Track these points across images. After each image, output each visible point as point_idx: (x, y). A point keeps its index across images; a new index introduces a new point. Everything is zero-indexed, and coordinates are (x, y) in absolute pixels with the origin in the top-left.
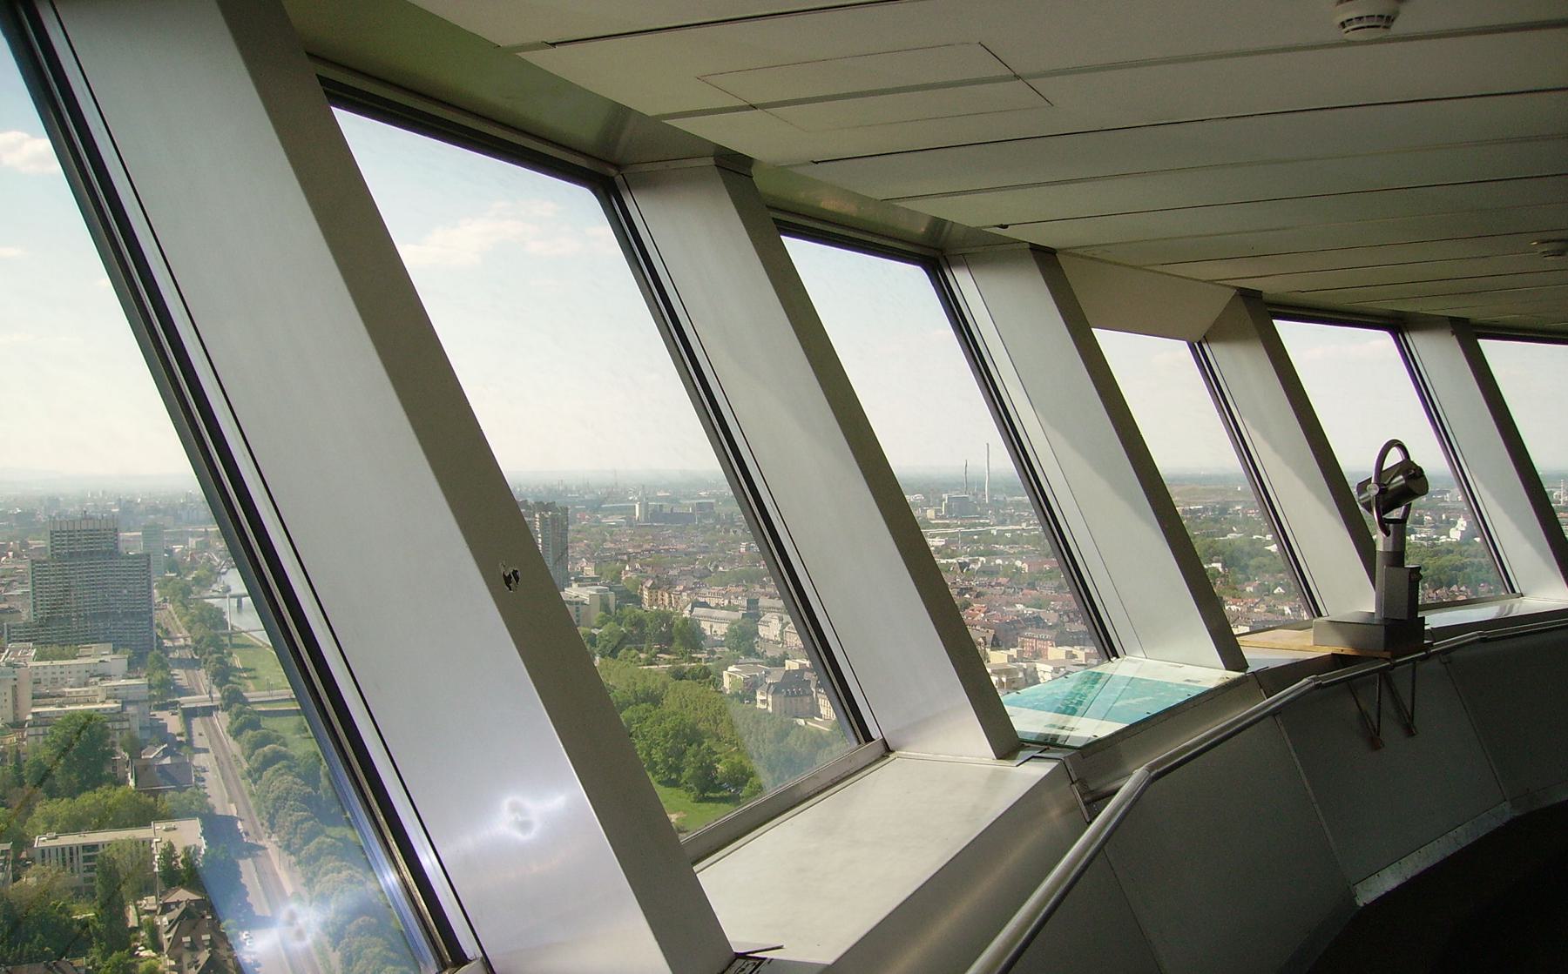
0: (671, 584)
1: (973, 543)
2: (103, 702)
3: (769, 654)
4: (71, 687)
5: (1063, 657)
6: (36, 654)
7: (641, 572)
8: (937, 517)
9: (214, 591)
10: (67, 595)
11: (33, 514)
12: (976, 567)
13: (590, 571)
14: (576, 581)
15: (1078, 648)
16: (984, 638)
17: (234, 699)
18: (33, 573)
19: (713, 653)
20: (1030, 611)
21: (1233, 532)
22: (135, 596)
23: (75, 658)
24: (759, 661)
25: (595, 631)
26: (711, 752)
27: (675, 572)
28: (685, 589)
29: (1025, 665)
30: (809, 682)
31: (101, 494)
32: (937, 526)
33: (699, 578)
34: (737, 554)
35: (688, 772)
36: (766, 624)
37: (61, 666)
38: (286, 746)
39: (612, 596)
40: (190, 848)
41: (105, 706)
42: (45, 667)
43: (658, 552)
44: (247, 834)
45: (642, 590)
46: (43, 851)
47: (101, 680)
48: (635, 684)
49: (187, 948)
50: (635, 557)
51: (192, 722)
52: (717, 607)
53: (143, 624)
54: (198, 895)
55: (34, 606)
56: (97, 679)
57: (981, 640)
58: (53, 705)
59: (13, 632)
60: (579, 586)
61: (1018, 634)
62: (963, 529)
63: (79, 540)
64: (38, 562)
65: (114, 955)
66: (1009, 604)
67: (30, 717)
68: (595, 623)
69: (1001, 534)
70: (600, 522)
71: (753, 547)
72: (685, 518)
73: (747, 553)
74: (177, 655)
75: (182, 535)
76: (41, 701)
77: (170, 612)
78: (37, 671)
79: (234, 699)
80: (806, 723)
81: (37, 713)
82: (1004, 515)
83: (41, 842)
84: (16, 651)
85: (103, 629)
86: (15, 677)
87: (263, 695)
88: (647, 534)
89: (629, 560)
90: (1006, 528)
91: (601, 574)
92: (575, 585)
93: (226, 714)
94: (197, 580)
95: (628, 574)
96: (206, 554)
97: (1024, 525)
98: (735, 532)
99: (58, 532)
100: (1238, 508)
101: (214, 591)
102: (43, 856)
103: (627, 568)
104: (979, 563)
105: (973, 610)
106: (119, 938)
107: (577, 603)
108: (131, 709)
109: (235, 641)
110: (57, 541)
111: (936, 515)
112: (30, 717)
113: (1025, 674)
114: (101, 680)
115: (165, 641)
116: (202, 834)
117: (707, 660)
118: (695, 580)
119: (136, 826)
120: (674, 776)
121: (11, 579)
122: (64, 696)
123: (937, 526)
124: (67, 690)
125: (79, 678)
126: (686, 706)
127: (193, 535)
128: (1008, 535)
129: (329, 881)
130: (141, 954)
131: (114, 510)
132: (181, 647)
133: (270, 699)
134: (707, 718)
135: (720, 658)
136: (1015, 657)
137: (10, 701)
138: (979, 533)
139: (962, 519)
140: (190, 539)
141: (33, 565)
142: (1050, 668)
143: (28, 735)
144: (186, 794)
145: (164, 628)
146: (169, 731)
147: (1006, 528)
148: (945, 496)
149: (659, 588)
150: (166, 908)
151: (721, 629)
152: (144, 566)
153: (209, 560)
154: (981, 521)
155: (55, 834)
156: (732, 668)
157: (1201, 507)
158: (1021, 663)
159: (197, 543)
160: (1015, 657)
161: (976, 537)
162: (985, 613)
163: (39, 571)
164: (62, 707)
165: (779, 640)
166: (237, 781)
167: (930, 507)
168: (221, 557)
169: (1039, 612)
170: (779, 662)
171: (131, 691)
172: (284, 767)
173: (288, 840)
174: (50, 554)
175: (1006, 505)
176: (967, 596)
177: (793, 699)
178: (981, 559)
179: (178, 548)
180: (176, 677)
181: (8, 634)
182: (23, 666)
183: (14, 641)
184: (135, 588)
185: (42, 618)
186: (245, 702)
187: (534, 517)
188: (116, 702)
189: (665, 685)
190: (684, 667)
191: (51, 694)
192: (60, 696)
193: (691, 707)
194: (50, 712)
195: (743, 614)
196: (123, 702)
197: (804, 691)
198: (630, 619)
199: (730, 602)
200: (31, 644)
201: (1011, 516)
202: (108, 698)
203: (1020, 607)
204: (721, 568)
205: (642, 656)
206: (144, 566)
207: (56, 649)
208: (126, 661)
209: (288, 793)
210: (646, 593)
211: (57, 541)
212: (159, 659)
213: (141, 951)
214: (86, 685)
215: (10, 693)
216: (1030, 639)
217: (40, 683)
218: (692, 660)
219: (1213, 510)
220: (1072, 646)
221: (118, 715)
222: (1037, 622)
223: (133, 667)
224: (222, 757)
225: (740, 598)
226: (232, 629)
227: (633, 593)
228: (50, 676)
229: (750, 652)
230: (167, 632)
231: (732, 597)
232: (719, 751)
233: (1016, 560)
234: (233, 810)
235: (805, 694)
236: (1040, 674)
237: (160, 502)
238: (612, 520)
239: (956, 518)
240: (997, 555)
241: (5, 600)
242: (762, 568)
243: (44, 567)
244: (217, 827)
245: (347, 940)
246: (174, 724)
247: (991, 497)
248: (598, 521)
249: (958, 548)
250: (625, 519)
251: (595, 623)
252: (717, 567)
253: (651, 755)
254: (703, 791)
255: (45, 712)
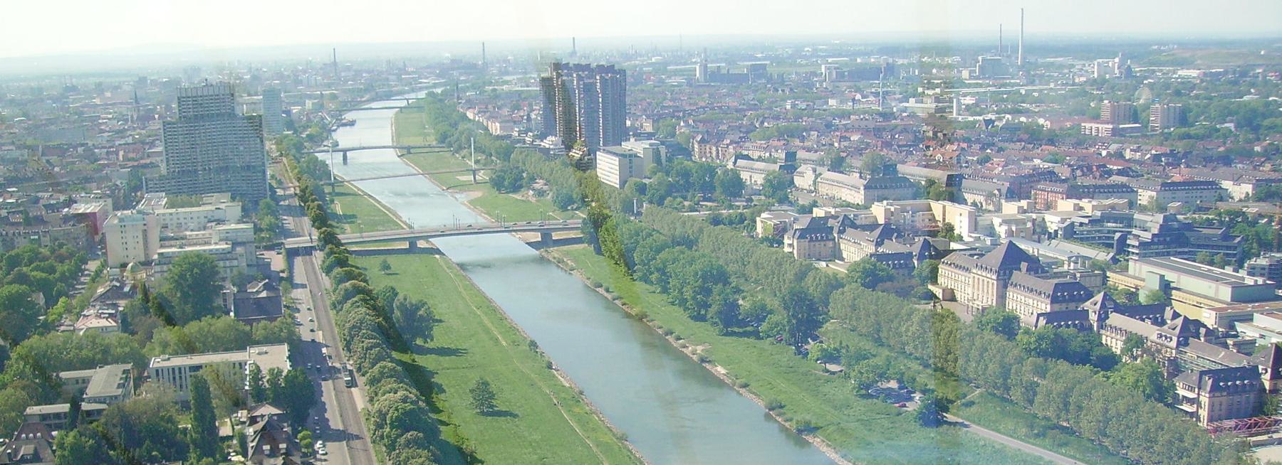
0: (720, 137)
1: (1001, 101)
2: (216, 244)
3: (801, 202)
4: (192, 230)
5: (1071, 209)
6: (166, 203)
7: (693, 127)
8: (970, 78)
9: (325, 146)
10: (194, 152)
11: (178, 82)
12: (999, 124)
13: (648, 127)
14: (634, 135)
15: (1086, 200)
16: (999, 190)
17: (329, 239)
18: (165, 133)
19: (752, 200)
20: (1047, 165)
21: (1251, 93)
22: (212, 150)
23: (200, 206)
24: (790, 208)
25: (646, 181)
26: (738, 291)
27: (725, 127)
28: (732, 142)
29: (1034, 216)
30: (832, 228)
31: (236, 64)
32: (969, 86)
33: (744, 133)
34: (784, 110)
35: (714, 309)
36: (802, 174)
37: (191, 213)
38: (366, 281)
39: (663, 150)
40: (274, 370)
41: (218, 247)
42: (171, 214)
43: (713, 109)
44: (330, 357)
45: (693, 144)
46: (157, 371)
47: (216, 224)
48: (675, 229)
49: (266, 455)
50: (690, 114)
51: (295, 260)
52: (760, 159)
53: (257, 176)
54: (279, 408)
55: (167, 162)
56: (213, 224)
57: (996, 192)
58: (175, 246)
59: (151, 184)
60: (636, 140)
61: (1031, 187)
62: (993, 89)
63: (201, 104)
64: (169, 124)
65: (204, 460)
66: (1026, 159)
67: (156, 257)
68: (648, 174)
69: (1028, 93)
70: (663, 83)
71: (797, 104)
72: (741, 78)
73: (792, 110)
74: (287, 203)
75: (301, 98)
76: (167, 243)
77: (285, 165)
78: (164, 217)
79: (329, 239)
80: (827, 265)
81: (162, 253)
82: (1033, 76)
83: (156, 362)
84: (150, 200)
85: (225, 181)
86: (145, 222)
87: (356, 237)
88: (704, 93)
89: (684, 116)
90: (1034, 88)
91: (658, 129)
92: (632, 140)
93: (322, 253)
94: (310, 137)
95: (682, 128)
96: (320, 114)
97: (1052, 85)
98: (783, 91)
99: (184, 98)
100: (1258, 71)
101: (325, 146)
102: (158, 375)
103: (682, 124)
104: (1004, 120)
105: (992, 164)
106: (211, 444)
107: (630, 156)
108: (239, 250)
109: (337, 190)
110: (183, 105)
111: (970, 76)
112: (156, 257)
113: (1033, 224)
114: (216, 224)
115: (278, 190)
116: (289, 358)
117: (745, 208)
118: (742, 135)
119: (236, 350)
120: (703, 312)
121: (155, 138)
122: (186, 238)
123: (969, 86)
124: (188, 233)
125: (199, 223)
126: (720, 249)
127: (310, 97)
128: (1036, 94)
129: (386, 400)
130: (233, 459)
131: (245, 77)
132: (291, 196)
133: (362, 240)
134: (736, 260)
135: (755, 205)
136: (1025, 208)
137: (141, 242)
138: (1008, 93)
139: (995, 79)
140: (307, 101)
141: (164, 126)
142: (1058, 219)
143: (155, 272)
144: (276, 323)
145: (278, 179)
146: (272, 269)
147: (1034, 88)
148: (980, 58)
149: (708, 142)
150: (253, 420)
151: (759, 179)
152: (257, 126)
153: (323, 119)
154: (1012, 81)
155: (167, 356)
156: (764, 215)
157: (1222, 70)
158: (1031, 214)
159: (313, 104)
160: (1025, 208)
161: (1005, 96)
162: (1003, 167)
163: (170, 131)
164: (182, 248)
165: (813, 189)
166: (326, 311)
167: (965, 68)
168: (332, 116)
169: (1054, 167)
170: (807, 210)
171: (239, 234)
172: (361, 300)
173: (360, 364)
174: (178, 117)
175: (1037, 66)
176: (989, 151)
177: (817, 243)
178: (1008, 116)
179: (295, 109)
180: (284, 222)
181: (147, 185)
182: (151, 213)
183: (151, 192)
184: (249, 141)
185: (174, 171)
186: (339, 244)
187: (572, 76)
188: (227, 244)
189: (701, 230)
190: (722, 214)
191: (175, 237)
192: (182, 238)
193: (723, 249)
194: (173, 252)
195: (781, 166)
196: (233, 244)
197: (827, 237)
198: (677, 171)
199: (770, 155)
200: (164, 194)
201: (1042, 76)
202: (221, 240)
203: (1037, 161)
204: (766, 124)
205: (686, 203)
206: (257, 126)
207: (185, 197)
208: (240, 208)
209: (361, 323)
210: (696, 146)
211: (183, 105)
212: (269, 206)
213: (233, 456)
214: (205, 228)
215: (141, 237)
216: (1042, 193)
217: (167, 227)
218: (731, 207)
219: (1234, 73)
220: (1080, 199)
221: (224, 255)
222: (1051, 176)
223: (246, 215)
224: (315, 290)
225: (780, 151)
226: (335, 178)
227: (684, 146)
228: (175, 221)
229: (784, 200)
230: (280, 182)
231: (773, 150)
232: (746, 289)
233: (1039, 118)
234: (319, 337)
235: (828, 239)
236: (1048, 224)
237: (285, 69)
238: (674, 81)
239: (989, 78)
240: (1022, 113)
241: (148, 156)
242: (804, 123)
243: (174, 128)
244: (303, 352)
245: (398, 451)
246: (277, 262)
247: (1024, 58)
248: (662, 81)
249: (987, 106)
250: (686, 79)
251: (648, 174)
252: (762, 123)
253: (682, 293)
254: (727, 325)
255: (168, 253)
